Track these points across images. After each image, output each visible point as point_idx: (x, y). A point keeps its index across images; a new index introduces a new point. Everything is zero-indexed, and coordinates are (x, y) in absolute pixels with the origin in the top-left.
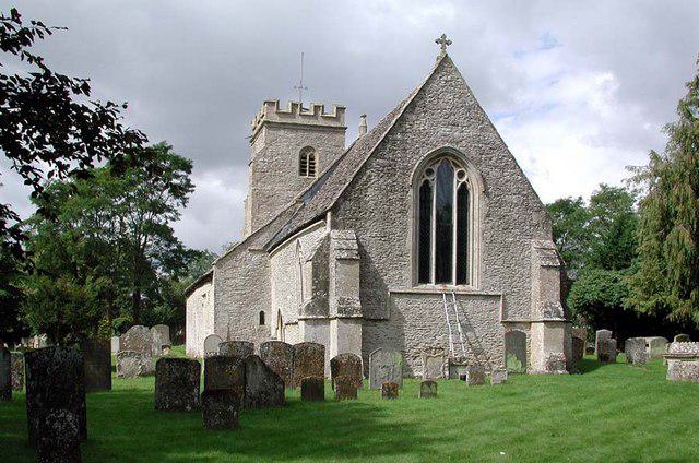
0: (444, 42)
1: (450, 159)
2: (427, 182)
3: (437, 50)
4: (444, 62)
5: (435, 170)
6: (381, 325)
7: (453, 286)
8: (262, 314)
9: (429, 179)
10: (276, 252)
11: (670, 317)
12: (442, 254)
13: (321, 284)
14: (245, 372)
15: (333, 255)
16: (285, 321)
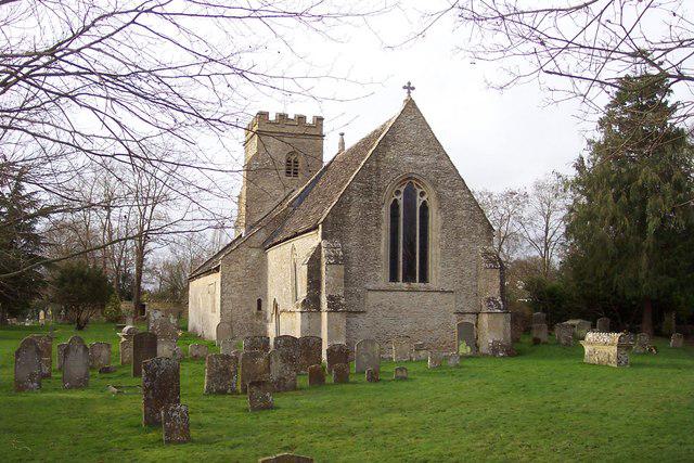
0: (409, 88)
1: (414, 181)
2: (396, 200)
3: (404, 95)
4: (410, 105)
5: (402, 191)
6: (360, 316)
7: (417, 285)
8: (259, 301)
9: (398, 198)
10: (289, 272)
11: (589, 165)
12: (409, 264)
13: (314, 282)
14: (269, 363)
15: (324, 261)
16: (280, 308)
